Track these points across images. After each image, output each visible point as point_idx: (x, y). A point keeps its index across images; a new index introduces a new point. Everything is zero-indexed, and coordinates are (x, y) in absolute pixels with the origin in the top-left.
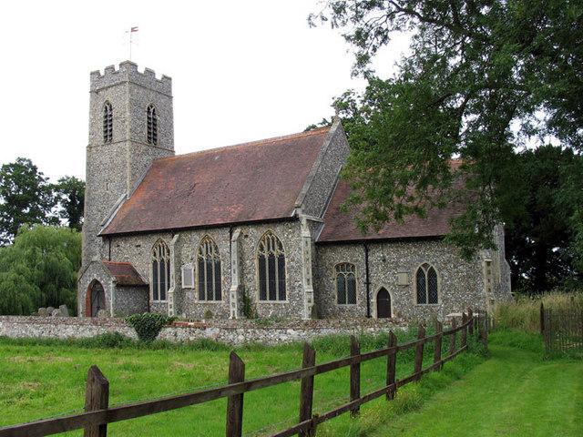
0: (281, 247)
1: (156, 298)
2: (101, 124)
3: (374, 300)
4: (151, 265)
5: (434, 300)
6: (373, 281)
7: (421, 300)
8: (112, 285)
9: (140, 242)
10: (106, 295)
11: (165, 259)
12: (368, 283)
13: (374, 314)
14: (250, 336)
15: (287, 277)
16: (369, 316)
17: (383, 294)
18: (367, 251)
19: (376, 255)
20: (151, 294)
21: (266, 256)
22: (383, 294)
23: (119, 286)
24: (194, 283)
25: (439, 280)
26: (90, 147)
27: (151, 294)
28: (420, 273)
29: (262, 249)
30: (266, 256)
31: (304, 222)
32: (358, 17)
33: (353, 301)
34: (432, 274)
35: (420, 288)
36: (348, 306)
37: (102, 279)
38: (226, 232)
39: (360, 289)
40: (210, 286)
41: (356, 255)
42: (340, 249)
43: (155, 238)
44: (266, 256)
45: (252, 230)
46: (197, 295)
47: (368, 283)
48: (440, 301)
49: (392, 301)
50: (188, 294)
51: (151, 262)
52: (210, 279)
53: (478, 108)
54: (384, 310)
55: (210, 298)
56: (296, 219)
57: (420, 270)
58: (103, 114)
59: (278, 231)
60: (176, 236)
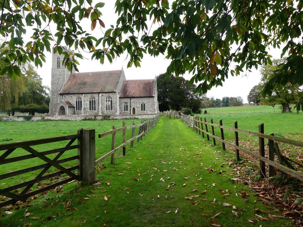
0: (95, 99)
1: (77, 110)
2: (56, 63)
3: (132, 110)
4: (75, 102)
5: (144, 110)
6: (132, 106)
7: (142, 110)
8: (67, 107)
9: (72, 96)
10: (65, 110)
11: (80, 100)
12: (130, 106)
13: (132, 113)
14: (120, 117)
15: (113, 105)
16: (130, 114)
17: (134, 109)
18: (130, 99)
19: (133, 100)
20: (75, 109)
21: (78, 101)
22: (134, 109)
23: (69, 107)
24: (88, 106)
25: (146, 106)
26: (52, 69)
27: (75, 109)
28: (142, 104)
29: (90, 99)
30: (91, 100)
31: (117, 93)
32: (58, 49)
33: (127, 110)
34: (144, 104)
35: (142, 107)
36: (126, 111)
37: (64, 106)
38: (97, 94)
39: (129, 107)
40: (93, 107)
41: (128, 100)
42: (125, 99)
43: (91, 94)
44: (91, 100)
45: (104, 94)
46: (89, 109)
47: (130, 106)
48: (146, 110)
49: (136, 110)
50: (87, 109)
51: (75, 101)
52: (92, 105)
53: (254, 55)
54: (134, 113)
55: (93, 110)
56: (115, 92)
57: (142, 104)
58: (57, 60)
59: (111, 95)
60: (83, 95)
